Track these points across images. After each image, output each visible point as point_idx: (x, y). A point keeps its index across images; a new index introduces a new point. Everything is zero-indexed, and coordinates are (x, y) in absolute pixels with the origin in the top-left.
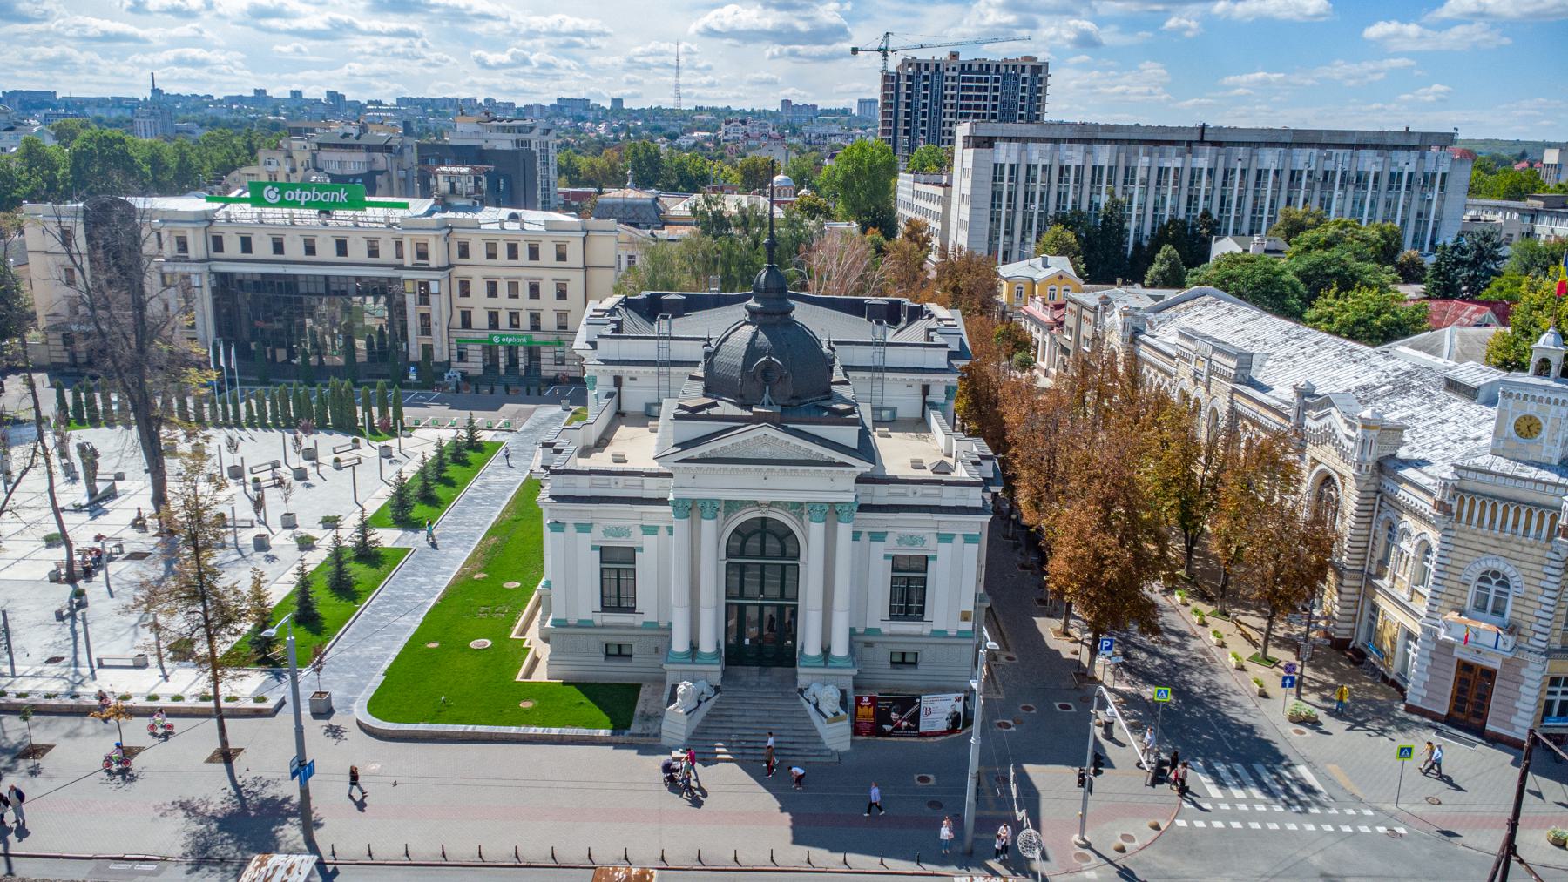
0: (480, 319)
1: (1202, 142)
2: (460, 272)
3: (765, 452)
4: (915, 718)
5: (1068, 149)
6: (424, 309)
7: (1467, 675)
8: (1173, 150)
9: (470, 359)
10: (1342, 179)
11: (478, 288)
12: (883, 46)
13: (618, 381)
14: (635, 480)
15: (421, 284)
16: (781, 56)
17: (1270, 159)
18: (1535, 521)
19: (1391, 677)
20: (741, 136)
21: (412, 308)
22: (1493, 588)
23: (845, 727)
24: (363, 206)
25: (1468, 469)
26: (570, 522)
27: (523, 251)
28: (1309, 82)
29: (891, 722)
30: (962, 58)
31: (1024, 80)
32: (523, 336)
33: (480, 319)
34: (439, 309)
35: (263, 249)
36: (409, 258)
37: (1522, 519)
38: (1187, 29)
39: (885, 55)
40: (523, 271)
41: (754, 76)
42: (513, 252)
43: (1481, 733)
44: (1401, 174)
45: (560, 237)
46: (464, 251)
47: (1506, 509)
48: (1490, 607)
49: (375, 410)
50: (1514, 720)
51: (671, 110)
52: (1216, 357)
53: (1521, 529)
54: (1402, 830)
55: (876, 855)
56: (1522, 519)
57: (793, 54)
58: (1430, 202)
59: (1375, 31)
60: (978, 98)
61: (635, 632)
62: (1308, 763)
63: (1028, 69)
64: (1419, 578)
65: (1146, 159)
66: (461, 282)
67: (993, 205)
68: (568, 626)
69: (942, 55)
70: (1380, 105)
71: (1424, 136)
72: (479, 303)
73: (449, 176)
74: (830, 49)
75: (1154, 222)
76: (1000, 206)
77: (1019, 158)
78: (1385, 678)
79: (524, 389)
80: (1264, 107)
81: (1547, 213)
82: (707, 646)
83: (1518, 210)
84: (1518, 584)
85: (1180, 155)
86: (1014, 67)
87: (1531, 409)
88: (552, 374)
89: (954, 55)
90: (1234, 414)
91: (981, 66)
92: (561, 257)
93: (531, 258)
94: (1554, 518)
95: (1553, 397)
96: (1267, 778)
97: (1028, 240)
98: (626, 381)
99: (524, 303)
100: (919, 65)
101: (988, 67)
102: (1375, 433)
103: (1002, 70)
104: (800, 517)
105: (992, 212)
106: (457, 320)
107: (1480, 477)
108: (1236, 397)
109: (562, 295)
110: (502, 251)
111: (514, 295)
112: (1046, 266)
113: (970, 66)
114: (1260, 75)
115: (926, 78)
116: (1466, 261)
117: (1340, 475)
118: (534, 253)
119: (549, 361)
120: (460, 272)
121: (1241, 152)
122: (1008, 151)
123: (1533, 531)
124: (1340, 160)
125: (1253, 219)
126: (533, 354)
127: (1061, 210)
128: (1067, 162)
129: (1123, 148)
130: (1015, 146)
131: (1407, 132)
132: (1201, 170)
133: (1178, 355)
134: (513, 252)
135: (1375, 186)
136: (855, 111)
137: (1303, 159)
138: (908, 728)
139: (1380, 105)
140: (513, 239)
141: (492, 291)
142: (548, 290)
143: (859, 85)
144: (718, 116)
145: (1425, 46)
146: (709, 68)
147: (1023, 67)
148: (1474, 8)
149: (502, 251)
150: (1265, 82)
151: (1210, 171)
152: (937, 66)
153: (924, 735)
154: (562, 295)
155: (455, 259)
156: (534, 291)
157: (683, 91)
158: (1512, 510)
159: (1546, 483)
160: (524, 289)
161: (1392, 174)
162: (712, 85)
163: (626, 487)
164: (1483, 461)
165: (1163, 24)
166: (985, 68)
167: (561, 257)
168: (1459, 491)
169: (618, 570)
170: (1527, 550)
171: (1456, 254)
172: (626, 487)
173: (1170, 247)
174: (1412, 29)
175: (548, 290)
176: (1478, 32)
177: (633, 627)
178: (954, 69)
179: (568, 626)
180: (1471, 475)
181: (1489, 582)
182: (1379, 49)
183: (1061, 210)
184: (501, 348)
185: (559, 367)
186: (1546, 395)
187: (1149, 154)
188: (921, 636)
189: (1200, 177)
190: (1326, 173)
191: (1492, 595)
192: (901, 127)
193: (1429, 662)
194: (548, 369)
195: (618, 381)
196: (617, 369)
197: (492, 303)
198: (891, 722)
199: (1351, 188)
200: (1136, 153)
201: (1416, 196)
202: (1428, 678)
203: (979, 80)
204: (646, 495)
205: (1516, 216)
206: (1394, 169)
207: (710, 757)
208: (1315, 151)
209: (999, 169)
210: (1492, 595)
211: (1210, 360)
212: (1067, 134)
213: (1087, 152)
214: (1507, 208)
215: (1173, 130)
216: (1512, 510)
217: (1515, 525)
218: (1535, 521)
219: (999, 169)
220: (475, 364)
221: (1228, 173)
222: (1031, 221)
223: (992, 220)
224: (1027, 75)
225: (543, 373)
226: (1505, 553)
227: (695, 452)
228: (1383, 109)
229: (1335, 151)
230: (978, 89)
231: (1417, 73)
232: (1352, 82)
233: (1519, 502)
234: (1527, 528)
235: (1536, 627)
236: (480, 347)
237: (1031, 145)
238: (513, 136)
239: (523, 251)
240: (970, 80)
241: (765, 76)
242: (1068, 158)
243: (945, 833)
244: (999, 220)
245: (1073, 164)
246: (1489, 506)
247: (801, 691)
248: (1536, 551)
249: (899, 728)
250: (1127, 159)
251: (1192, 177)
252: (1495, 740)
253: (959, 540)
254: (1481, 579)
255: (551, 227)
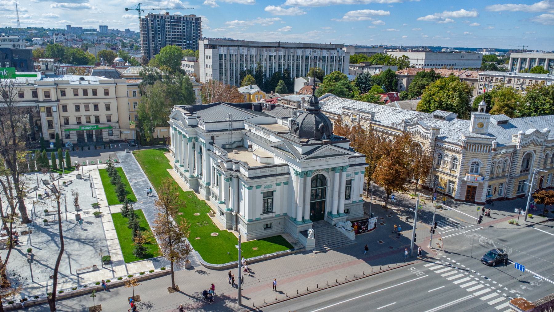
0: (73, 120)
1: (279, 47)
2: (62, 102)
3: (326, 153)
4: (367, 227)
5: (243, 49)
6: (50, 118)
7: (470, 189)
8: (273, 49)
9: (71, 137)
10: (319, 58)
11: (71, 108)
12: (138, 8)
13: (213, 138)
14: (274, 168)
15: (47, 108)
16: (57, 7)
17: (300, 52)
18: (485, 148)
19: (446, 193)
20: (63, 40)
21: (44, 118)
22: (475, 166)
23: (353, 233)
24: (15, 76)
25: (469, 137)
26: (254, 186)
27: (90, 92)
28: (251, 24)
29: (361, 229)
30: (170, 14)
31: (193, 23)
32: (92, 127)
33: (73, 120)
34: (56, 119)
35: (28, 96)
36: (41, 97)
37: (482, 148)
38: (212, 5)
39: (140, 12)
40: (91, 100)
41: (46, 15)
42: (85, 93)
43: (474, 202)
44: (333, 57)
45: (106, 86)
46: (63, 93)
47: (478, 146)
48: (474, 171)
49: (58, 161)
50: (482, 198)
51: (16, 29)
52: (361, 114)
53: (482, 150)
54: (482, 228)
55: (394, 263)
56: (482, 148)
57: (63, 6)
58: (341, 65)
59: (269, 8)
60: (178, 29)
61: (273, 219)
62: (450, 217)
63: (194, 19)
64: (452, 167)
65: (266, 52)
66: (63, 107)
67: (220, 69)
68: (253, 221)
69: (163, 12)
70: (272, 32)
71: (337, 45)
72: (72, 114)
73: (44, 63)
74: (78, 5)
75: (269, 73)
76: (222, 69)
77: (227, 52)
78: (444, 194)
79: (103, 147)
80: (240, 32)
81: (366, 67)
82: (307, 217)
83: (358, 66)
84: (481, 164)
85: (276, 51)
86: (189, 18)
87: (481, 120)
88: (108, 140)
89: (168, 13)
90: (372, 129)
91: (178, 17)
92: (107, 93)
93: (84, 95)
94: (490, 147)
95: (486, 117)
96: (447, 223)
97: (232, 80)
98: (215, 138)
99: (92, 113)
100: (155, 16)
101: (180, 18)
102: (435, 131)
103: (185, 19)
104: (328, 172)
105: (220, 71)
106: (63, 122)
107: (472, 139)
108: (372, 125)
109: (108, 108)
110: (81, 92)
111: (87, 109)
112: (252, 88)
113: (174, 17)
114: (236, 21)
115: (158, 21)
116: (363, 82)
117: (422, 143)
118: (95, 93)
119: (106, 135)
120: (62, 102)
121: (292, 50)
122: (224, 50)
123: (485, 151)
124: (319, 53)
125: (270, 71)
126: (99, 133)
127: (242, 70)
128: (242, 54)
129: (259, 49)
130: (226, 48)
131: (225, 39)
132: (281, 56)
133: (343, 114)
134: (85, 93)
135: (327, 61)
136: (98, 30)
137: (308, 52)
138: (366, 230)
139: (272, 32)
140: (85, 88)
141: (78, 108)
142: (102, 107)
143: (93, 20)
144: (39, 31)
145: (283, 14)
146: (26, 11)
147: (192, 18)
148: (295, 3)
149: (81, 92)
150: (238, 24)
151: (284, 56)
152: (162, 17)
153: (369, 231)
154: (108, 108)
155: (60, 97)
156: (96, 108)
157: (20, 21)
158: (480, 146)
159: (487, 138)
160: (92, 107)
161: (331, 57)
162: (28, 18)
163: (271, 171)
164: (471, 135)
165: (203, 3)
166: (179, 18)
167: (107, 93)
168: (467, 143)
169: (267, 199)
170: (484, 155)
171: (360, 80)
172: (271, 171)
173: (282, 81)
174: (278, 8)
175: (102, 107)
176: (297, 10)
177: (272, 217)
178: (168, 18)
179: (253, 221)
180: (470, 138)
181: (474, 165)
182: (270, 14)
183: (242, 70)
184: (85, 131)
185: (111, 137)
186: (485, 117)
187: (266, 51)
188: (350, 204)
189: (281, 58)
190: (315, 56)
191: (475, 168)
192: (151, 39)
193: (460, 187)
194: (106, 137)
195: (213, 138)
196: (211, 134)
197: (78, 114)
198: (361, 229)
199: (321, 61)
200: (263, 51)
201: (337, 63)
202: (460, 191)
203: (178, 22)
204: (278, 173)
205: (357, 68)
206: (332, 55)
207: (324, 250)
208: (311, 50)
209: (221, 56)
210: (475, 168)
211: (359, 115)
212: (302, 46)
213: (248, 50)
214: (355, 66)
215: (271, 43)
216: (480, 146)
217: (481, 150)
218: (485, 148)
219: (221, 56)
220: (74, 138)
221: (289, 57)
222: (233, 73)
223: (220, 73)
224: (194, 21)
225: (104, 140)
226: (478, 157)
227: (310, 156)
228: (273, 34)
229: (317, 50)
230: (178, 26)
231: (282, 22)
232: (264, 25)
233: (481, 144)
234: (483, 150)
235: (486, 174)
236: (75, 132)
237: (230, 48)
238: (12, 43)
239: (90, 92)
240: (174, 22)
241: (51, 15)
242: (242, 52)
243: (406, 253)
244: (222, 73)
245: (244, 54)
246: (474, 145)
247: (335, 225)
248: (486, 155)
249: (363, 230)
250: (260, 53)
251: (279, 58)
252: (478, 204)
253: (360, 173)
254: (472, 164)
255: (101, 82)
